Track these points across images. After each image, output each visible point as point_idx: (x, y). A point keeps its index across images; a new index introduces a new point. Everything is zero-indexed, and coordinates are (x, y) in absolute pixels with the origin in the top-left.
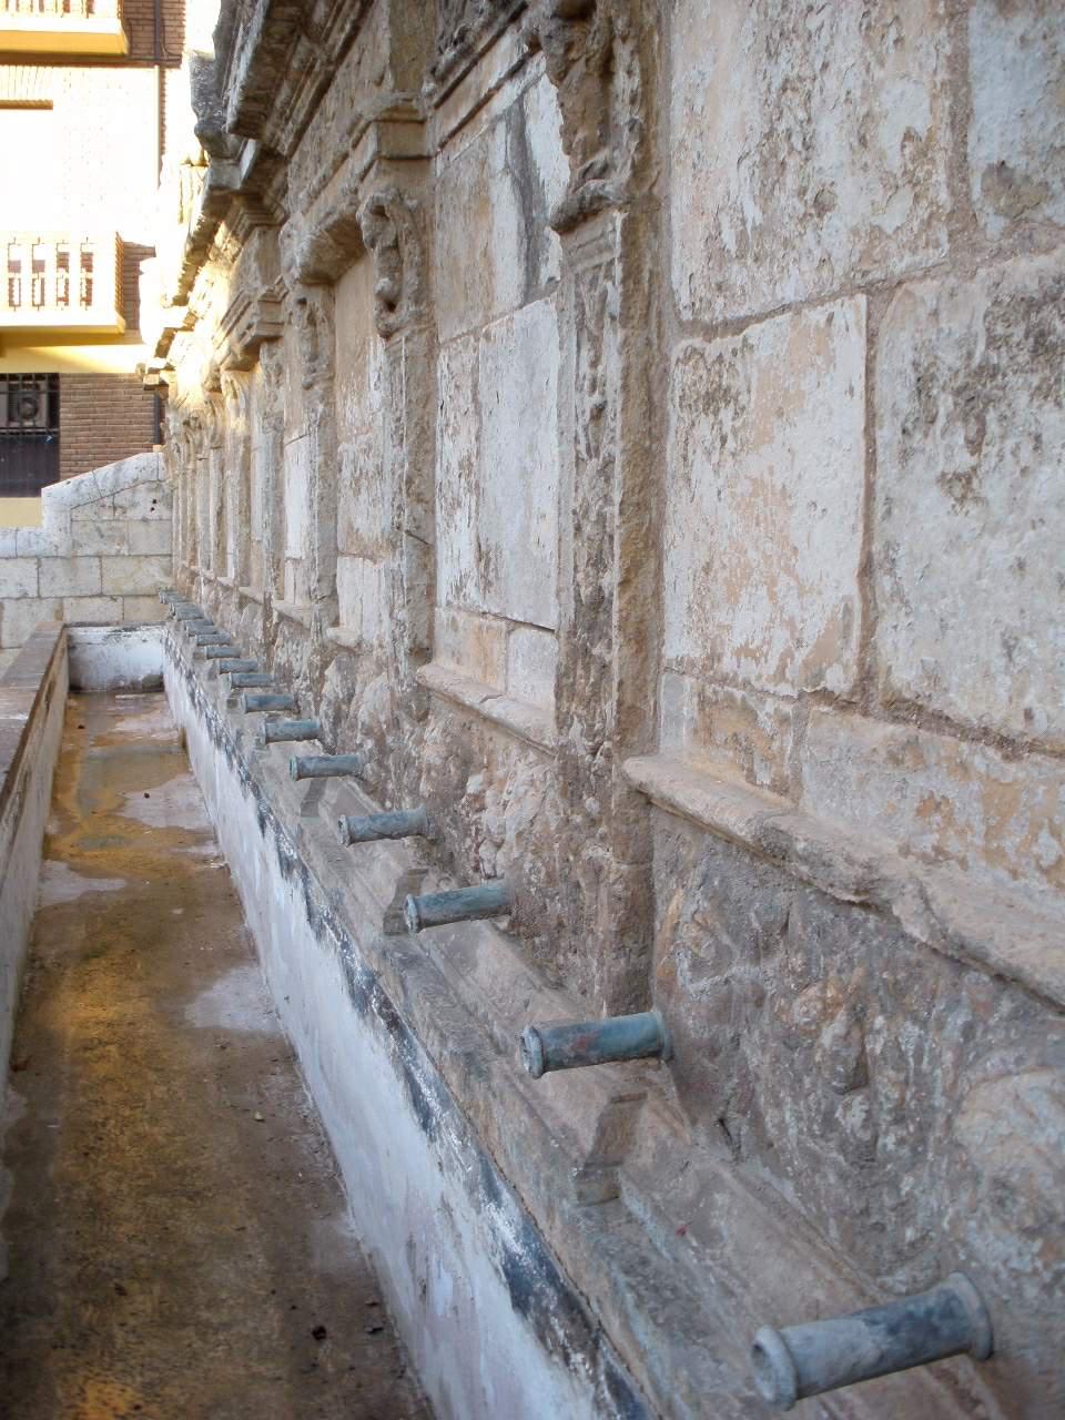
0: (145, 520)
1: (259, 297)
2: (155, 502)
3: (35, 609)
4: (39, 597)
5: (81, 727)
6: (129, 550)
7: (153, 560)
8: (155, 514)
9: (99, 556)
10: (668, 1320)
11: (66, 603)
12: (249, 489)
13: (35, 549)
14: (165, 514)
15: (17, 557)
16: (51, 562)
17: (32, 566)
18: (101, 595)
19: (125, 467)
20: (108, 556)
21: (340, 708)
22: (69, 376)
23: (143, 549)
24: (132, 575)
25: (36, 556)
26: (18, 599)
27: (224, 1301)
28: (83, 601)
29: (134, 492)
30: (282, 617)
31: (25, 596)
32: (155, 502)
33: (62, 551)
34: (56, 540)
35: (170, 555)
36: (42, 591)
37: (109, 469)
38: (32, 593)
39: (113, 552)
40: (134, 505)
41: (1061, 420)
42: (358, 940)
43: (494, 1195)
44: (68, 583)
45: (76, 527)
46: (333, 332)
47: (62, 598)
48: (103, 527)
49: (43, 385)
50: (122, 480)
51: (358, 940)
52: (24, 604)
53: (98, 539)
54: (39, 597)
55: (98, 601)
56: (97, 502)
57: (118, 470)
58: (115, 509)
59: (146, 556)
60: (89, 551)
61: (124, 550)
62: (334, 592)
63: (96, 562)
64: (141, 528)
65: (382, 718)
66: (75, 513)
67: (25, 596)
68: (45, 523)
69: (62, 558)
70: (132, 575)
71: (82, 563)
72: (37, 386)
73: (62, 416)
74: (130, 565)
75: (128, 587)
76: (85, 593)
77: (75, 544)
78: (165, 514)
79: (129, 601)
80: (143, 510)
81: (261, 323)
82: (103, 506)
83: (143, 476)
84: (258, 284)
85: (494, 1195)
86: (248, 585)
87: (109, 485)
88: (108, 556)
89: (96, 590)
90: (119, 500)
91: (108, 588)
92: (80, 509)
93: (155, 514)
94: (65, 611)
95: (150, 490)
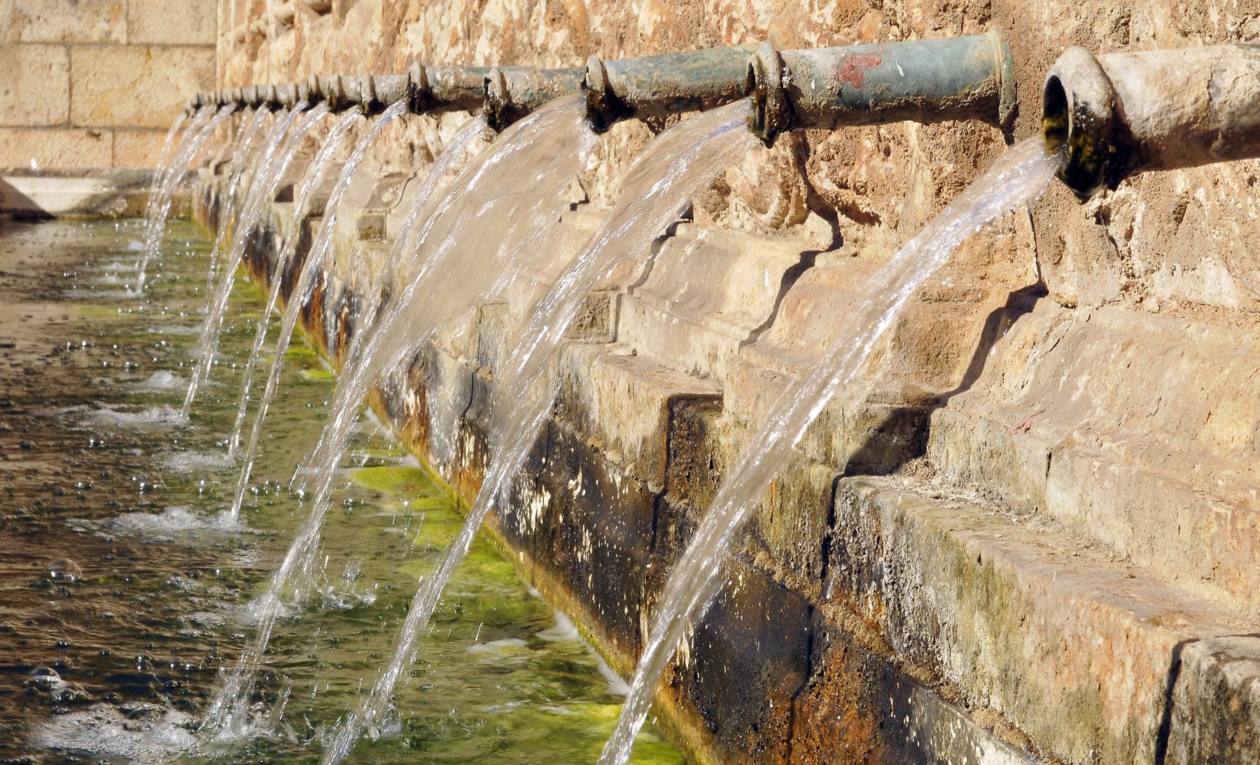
5: (855, 255)
6: (129, 33)
7: (177, 55)
9: (66, 43)
10: (316, 464)
18: (68, 125)
20: (86, 45)
23: (155, 30)
24: (133, 84)
27: (345, 578)
28: (34, 137)
35: (212, 47)
39: (96, 36)
41: (624, 97)
43: (31, 586)
59: (164, 47)
60: (47, 31)
61: (119, 32)
63: (58, 57)
70: (133, 84)
71: (31, 55)
74: (130, 65)
75: (123, 111)
76: (33, 119)
79: (125, 140)
85: (31, 586)
88: (86, 45)
89: (57, 116)
91: (83, 110)
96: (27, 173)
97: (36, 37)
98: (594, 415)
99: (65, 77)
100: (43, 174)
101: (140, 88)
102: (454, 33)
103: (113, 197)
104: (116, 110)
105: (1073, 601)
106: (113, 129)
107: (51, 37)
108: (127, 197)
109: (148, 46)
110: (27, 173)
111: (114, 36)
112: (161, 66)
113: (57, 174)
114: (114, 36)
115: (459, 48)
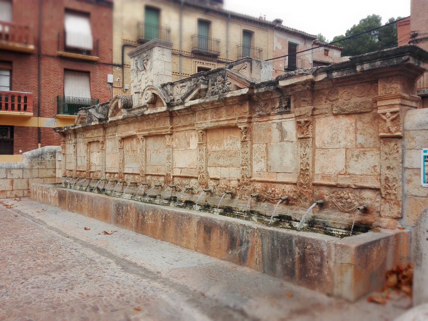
0: (49, 161)
9: (38, 169)
11: (30, 179)
13: (22, 167)
15: (17, 169)
18: (38, 178)
25: (22, 169)
28: (34, 179)
30: (173, 177)
31: (19, 178)
38: (21, 177)
40: (46, 157)
55: (38, 179)
60: (35, 167)
61: (44, 167)
63: (37, 170)
74: (46, 171)
75: (45, 176)
78: (54, 159)
79: (45, 179)
91: (40, 176)
93: (51, 160)
95: (50, 154)
112: (49, 171)
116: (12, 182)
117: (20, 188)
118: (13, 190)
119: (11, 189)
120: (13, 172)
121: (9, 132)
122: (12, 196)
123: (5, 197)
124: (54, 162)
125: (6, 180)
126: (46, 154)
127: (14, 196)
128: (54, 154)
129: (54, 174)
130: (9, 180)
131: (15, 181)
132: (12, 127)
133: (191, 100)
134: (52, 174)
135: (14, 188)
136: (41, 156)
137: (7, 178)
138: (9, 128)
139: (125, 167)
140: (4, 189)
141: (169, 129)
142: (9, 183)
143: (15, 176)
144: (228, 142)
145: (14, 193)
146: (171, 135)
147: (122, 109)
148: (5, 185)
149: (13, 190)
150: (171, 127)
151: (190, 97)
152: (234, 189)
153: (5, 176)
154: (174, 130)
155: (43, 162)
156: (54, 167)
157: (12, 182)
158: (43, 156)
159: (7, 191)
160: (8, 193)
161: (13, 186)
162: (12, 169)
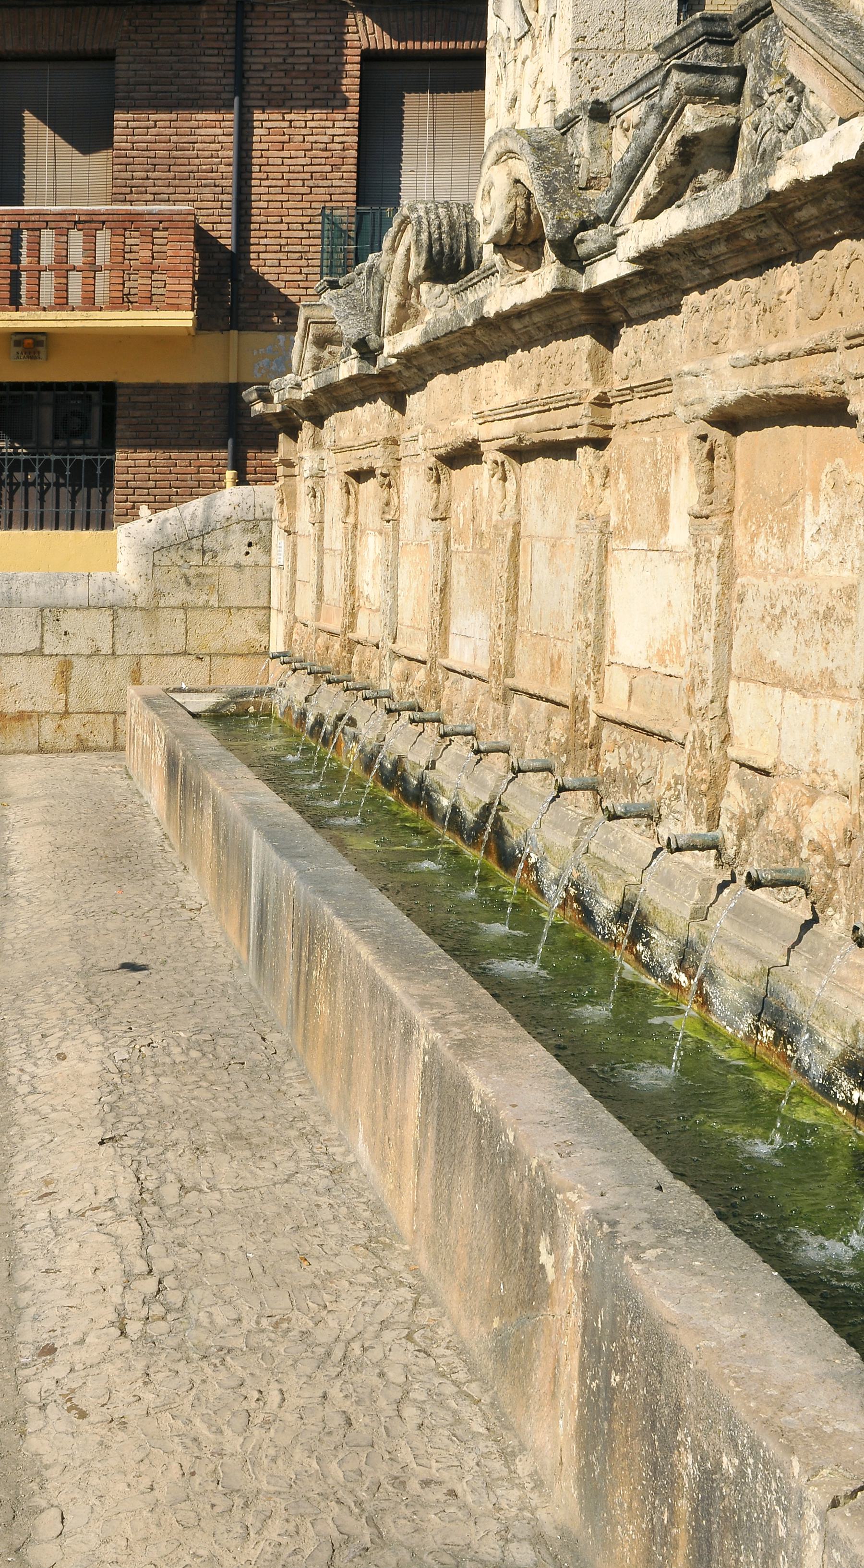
0: (239, 566)
1: (591, 398)
2: (250, 545)
3: (108, 667)
4: (113, 654)
8: (249, 560)
9: (184, 607)
11: (144, 662)
12: (517, 575)
13: (110, 598)
14: (262, 560)
15: (89, 607)
16: (128, 613)
17: (106, 617)
18: (185, 653)
19: (218, 502)
21: (745, 821)
22: (128, 386)
25: (111, 607)
26: (89, 656)
28: (166, 660)
29: (226, 533)
30: (602, 718)
31: (96, 653)
32: (250, 545)
33: (141, 601)
34: (135, 587)
36: (118, 646)
37: (195, 506)
38: (106, 649)
40: (226, 548)
42: (505, 1039)
44: (146, 639)
45: (158, 573)
46: (734, 468)
47: (140, 656)
48: (191, 572)
49: (95, 395)
50: (214, 518)
51: (505, 1039)
52: (96, 662)
53: (185, 586)
54: (113, 654)
55: (182, 661)
56: (184, 544)
57: (209, 507)
58: (204, 553)
59: (239, 609)
60: (173, 602)
61: (214, 601)
62: (725, 711)
63: (180, 615)
64: (234, 574)
65: (833, 837)
66: (158, 556)
67: (96, 653)
68: (120, 567)
69: (142, 609)
71: (164, 614)
72: (89, 397)
73: (118, 435)
74: (219, 619)
75: (216, 645)
77: (158, 593)
78: (262, 560)
79: (217, 661)
80: (235, 555)
81: (592, 424)
82: (191, 549)
83: (237, 515)
84: (589, 385)
86: (513, 676)
87: (198, 524)
90: (209, 542)
91: (193, 645)
92: (164, 552)
93: (249, 560)
94: (143, 672)
95: (245, 531)
96: (181, 690)
97: (167, 604)
98: (73, 671)
99: (184, 626)
100: (189, 691)
101: (225, 632)
102: (669, 784)
103: (229, 703)
104: (212, 644)
105: (233, 1241)
106: (210, 655)
107: (176, 604)
108: (236, 703)
109: (230, 608)
110: (181, 690)
111: (210, 603)
112: (237, 619)
113: (197, 691)
114: (210, 603)
115: (672, 792)
116: (65, 669)
117: (100, 704)
118: (66, 713)
119: (60, 707)
120: (69, 621)
121: (96, 414)
122: (64, 744)
123: (33, 744)
124: (263, 573)
125: (39, 663)
126: (226, 529)
127: (71, 743)
128: (257, 528)
129: (263, 638)
130: (53, 663)
131: (79, 666)
132: (109, 389)
133: (649, 212)
134: (253, 633)
135: (73, 707)
136: (196, 542)
137: (39, 652)
138: (95, 395)
139: (453, 629)
140: (27, 707)
141: (582, 410)
142: (51, 676)
143: (79, 645)
144: (824, 513)
145: (74, 725)
146: (600, 444)
147: (424, 287)
148: (30, 686)
149: (66, 713)
150: (595, 393)
151: (637, 201)
152: (819, 858)
153: (36, 644)
154: (615, 415)
155: (209, 571)
156: (262, 602)
157: (65, 669)
158: (209, 542)
159: (40, 716)
160: (48, 726)
161: (66, 690)
162: (65, 608)
